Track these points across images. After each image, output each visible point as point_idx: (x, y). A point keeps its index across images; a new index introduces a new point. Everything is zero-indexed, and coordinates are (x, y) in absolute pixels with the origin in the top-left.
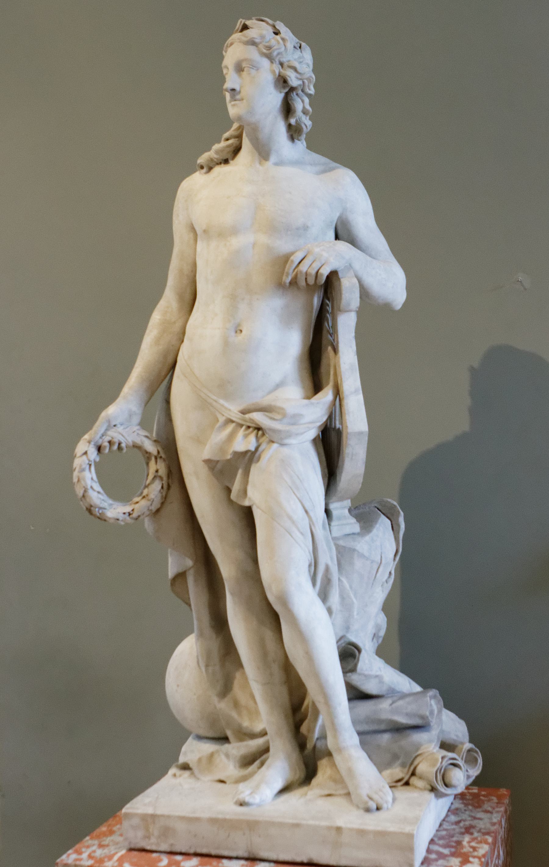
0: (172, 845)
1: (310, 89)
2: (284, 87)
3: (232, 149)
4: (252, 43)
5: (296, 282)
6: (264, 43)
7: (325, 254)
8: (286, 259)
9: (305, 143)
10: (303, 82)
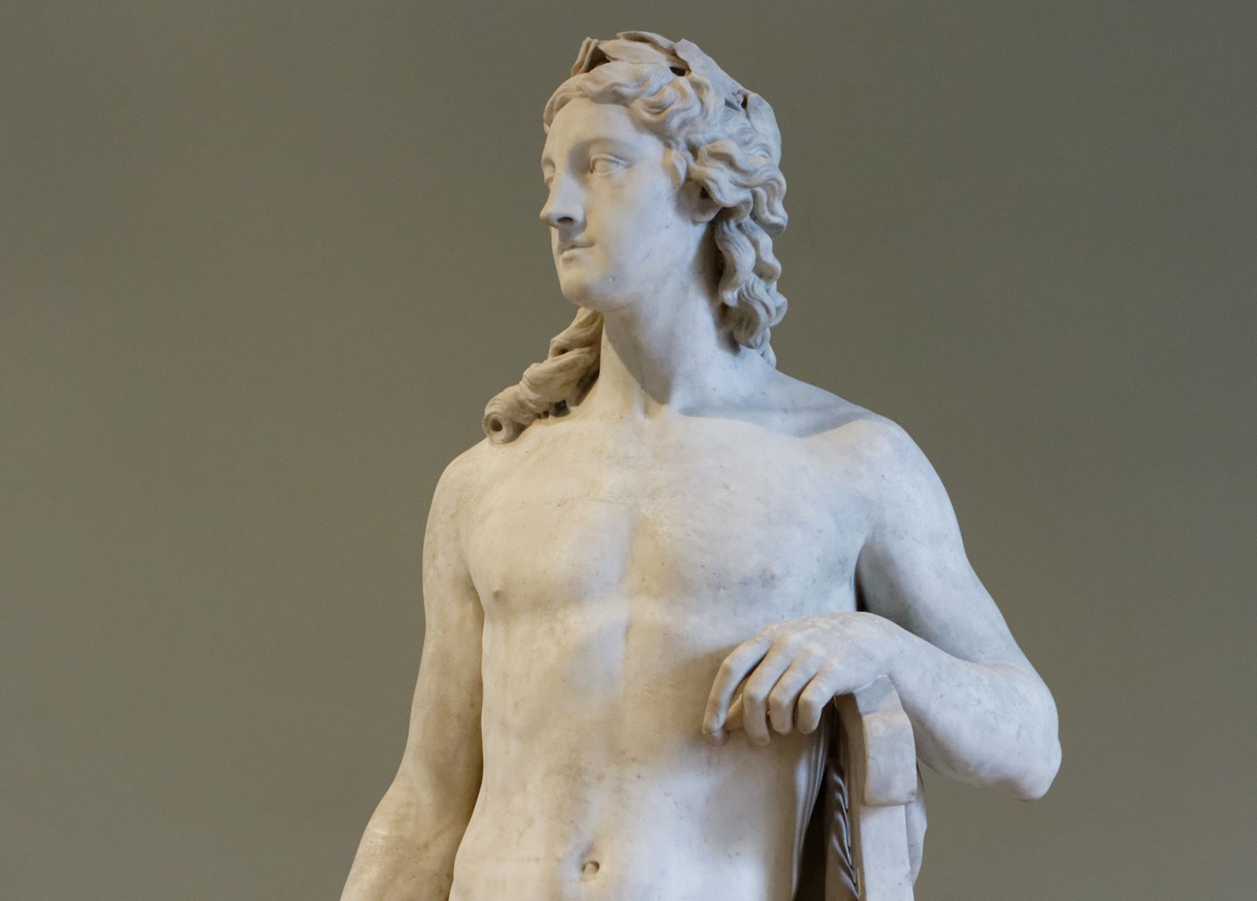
1: (773, 213)
2: (703, 210)
3: (575, 375)
4: (616, 97)
5: (742, 729)
6: (645, 97)
7: (817, 650)
8: (714, 662)
9: (771, 355)
10: (755, 195)
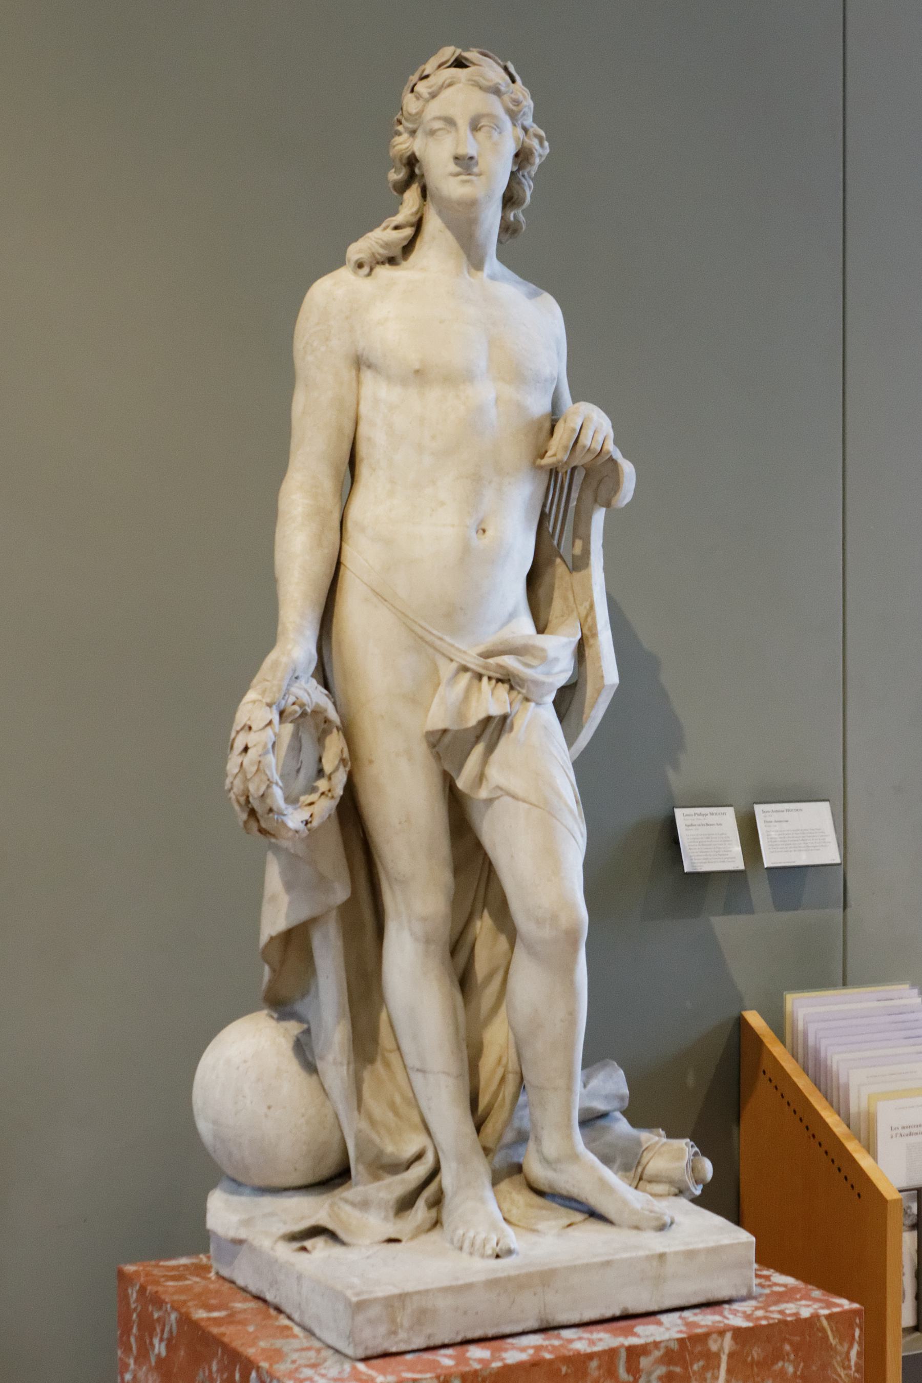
0: (429, 1337)
